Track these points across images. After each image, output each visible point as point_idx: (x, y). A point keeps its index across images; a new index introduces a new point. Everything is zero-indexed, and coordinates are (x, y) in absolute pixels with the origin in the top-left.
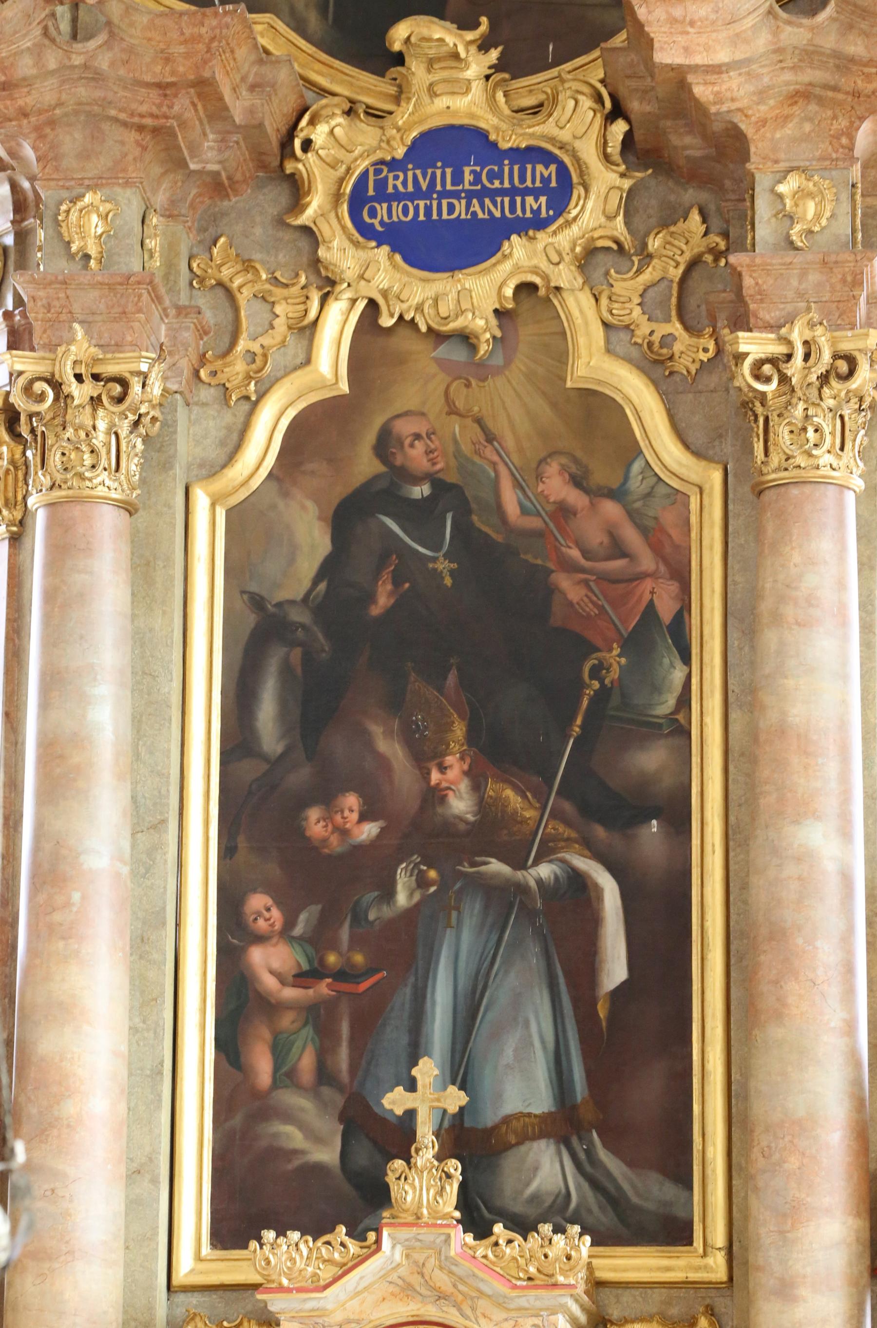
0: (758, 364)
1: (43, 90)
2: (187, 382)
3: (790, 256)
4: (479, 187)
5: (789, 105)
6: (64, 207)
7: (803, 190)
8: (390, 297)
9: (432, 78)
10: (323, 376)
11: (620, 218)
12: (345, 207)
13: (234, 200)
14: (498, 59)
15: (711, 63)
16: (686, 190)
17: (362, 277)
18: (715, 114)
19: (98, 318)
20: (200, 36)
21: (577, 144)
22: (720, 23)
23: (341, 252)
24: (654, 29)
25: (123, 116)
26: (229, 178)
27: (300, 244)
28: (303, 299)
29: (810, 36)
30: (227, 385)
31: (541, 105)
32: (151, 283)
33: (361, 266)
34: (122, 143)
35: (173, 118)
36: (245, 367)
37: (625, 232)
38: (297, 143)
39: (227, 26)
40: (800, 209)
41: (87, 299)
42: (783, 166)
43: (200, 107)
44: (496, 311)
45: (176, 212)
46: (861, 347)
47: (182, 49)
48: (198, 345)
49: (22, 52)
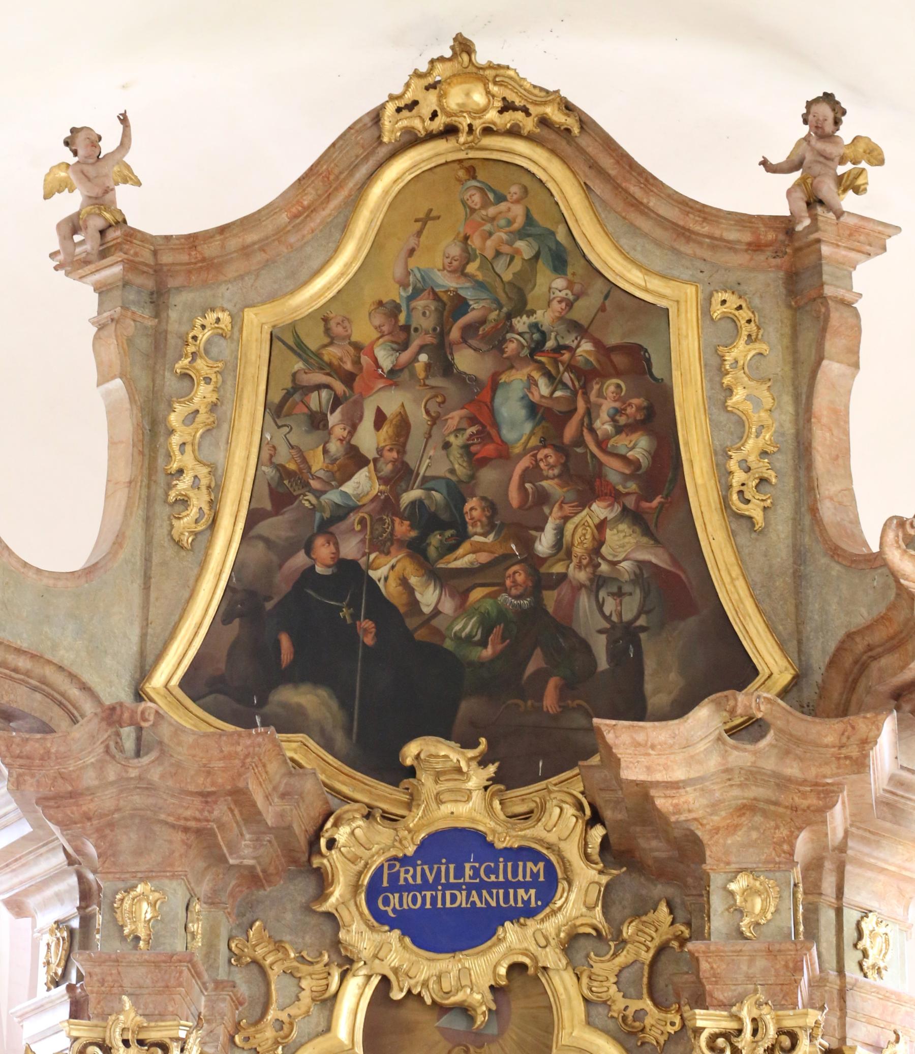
0: (713, 1037)
1: (104, 798)
2: (223, 1047)
3: (740, 944)
4: (478, 881)
5: (738, 816)
6: (119, 896)
7: (751, 889)
8: (400, 973)
9: (439, 788)
10: (341, 1043)
11: (599, 908)
12: (363, 896)
13: (268, 889)
14: (495, 773)
15: (669, 780)
16: (655, 885)
17: (376, 956)
18: (675, 823)
19: (145, 991)
20: (237, 753)
21: (562, 845)
22: (677, 747)
23: (360, 935)
24: (621, 751)
25: (171, 819)
26: (264, 871)
27: (324, 928)
28: (325, 975)
29: (754, 759)
30: (258, 1049)
31: (532, 812)
32: (190, 961)
33: (376, 947)
34: (170, 842)
35: (213, 821)
36: (275, 1033)
37: (603, 920)
38: (323, 842)
39: (259, 745)
40: (749, 905)
41: (136, 975)
42: (734, 867)
43: (236, 812)
44: (491, 987)
45: (217, 900)
46: (801, 1025)
47: (221, 764)
48: (234, 1015)
49: (87, 766)
